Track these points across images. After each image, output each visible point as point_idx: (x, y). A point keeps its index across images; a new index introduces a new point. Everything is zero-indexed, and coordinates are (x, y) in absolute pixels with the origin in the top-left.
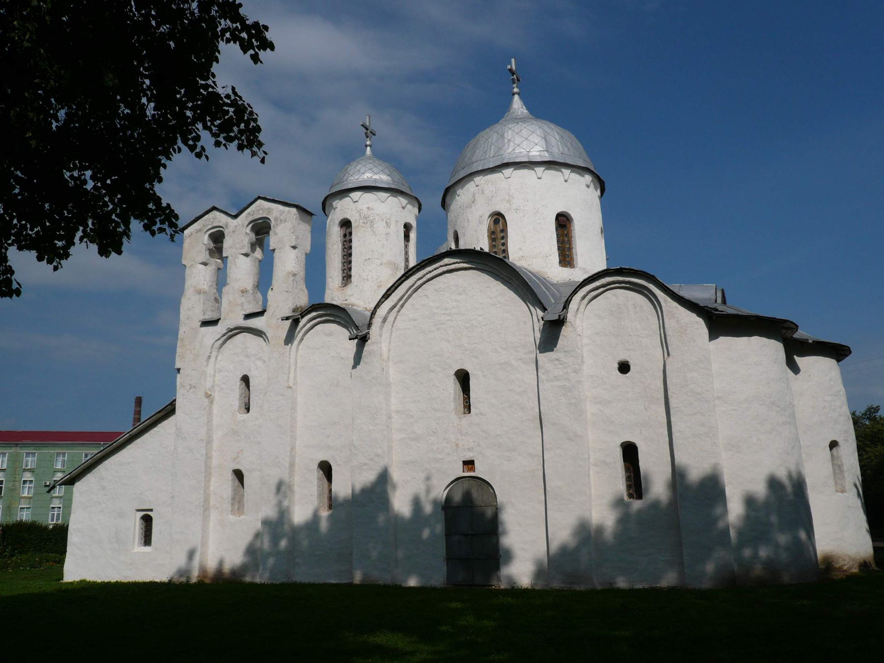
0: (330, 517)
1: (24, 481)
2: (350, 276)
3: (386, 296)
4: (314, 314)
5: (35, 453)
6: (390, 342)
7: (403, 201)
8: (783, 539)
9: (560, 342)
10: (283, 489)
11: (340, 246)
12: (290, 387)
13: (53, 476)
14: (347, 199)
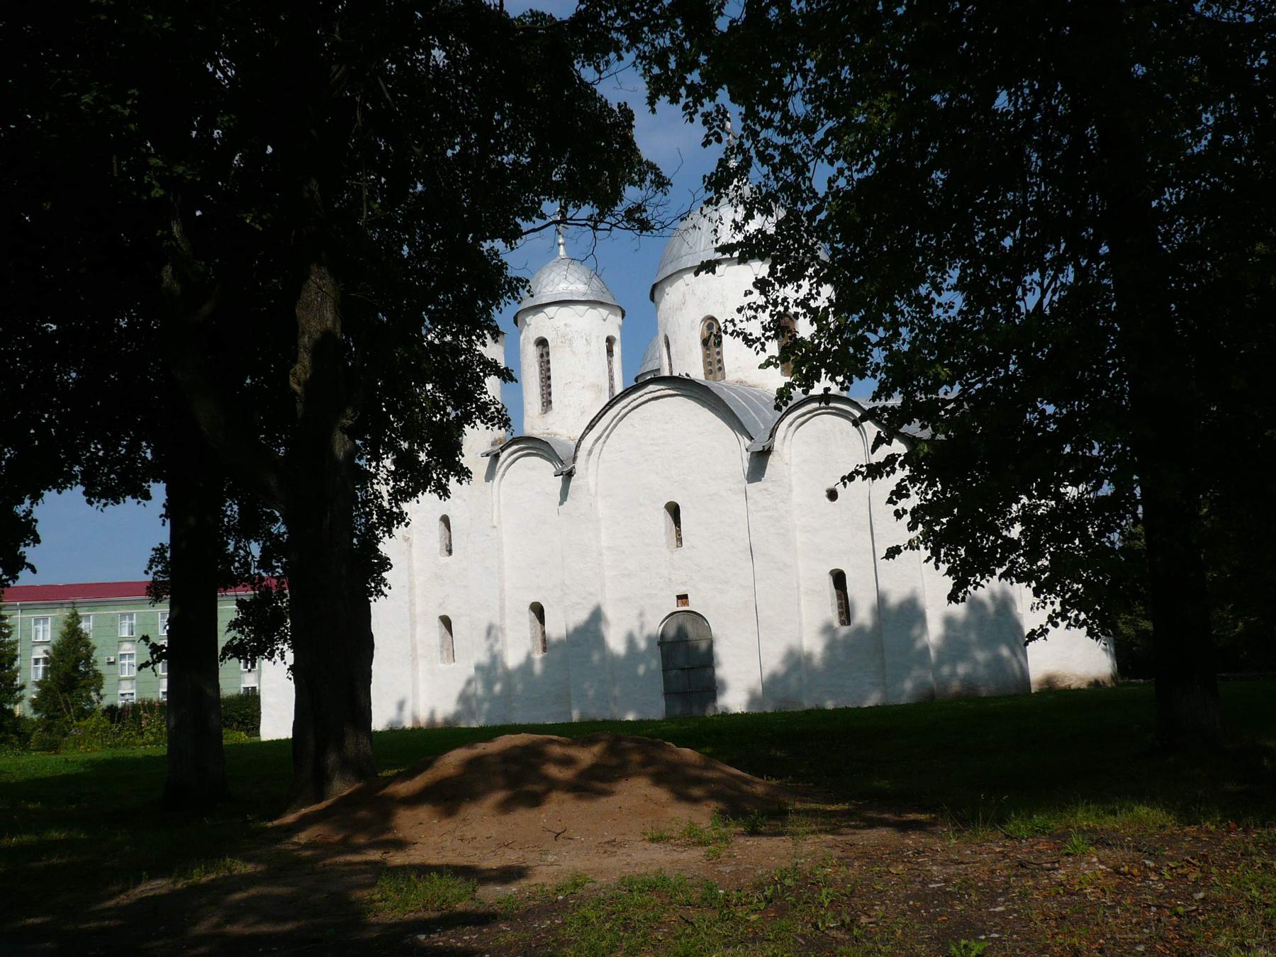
0: (544, 660)
1: (121, 655)
2: (550, 402)
3: (591, 427)
4: (515, 447)
5: (89, 616)
6: (597, 475)
7: (604, 312)
8: (981, 656)
9: (767, 471)
10: (493, 632)
11: (537, 368)
12: (495, 527)
13: (119, 647)
14: (541, 315)
